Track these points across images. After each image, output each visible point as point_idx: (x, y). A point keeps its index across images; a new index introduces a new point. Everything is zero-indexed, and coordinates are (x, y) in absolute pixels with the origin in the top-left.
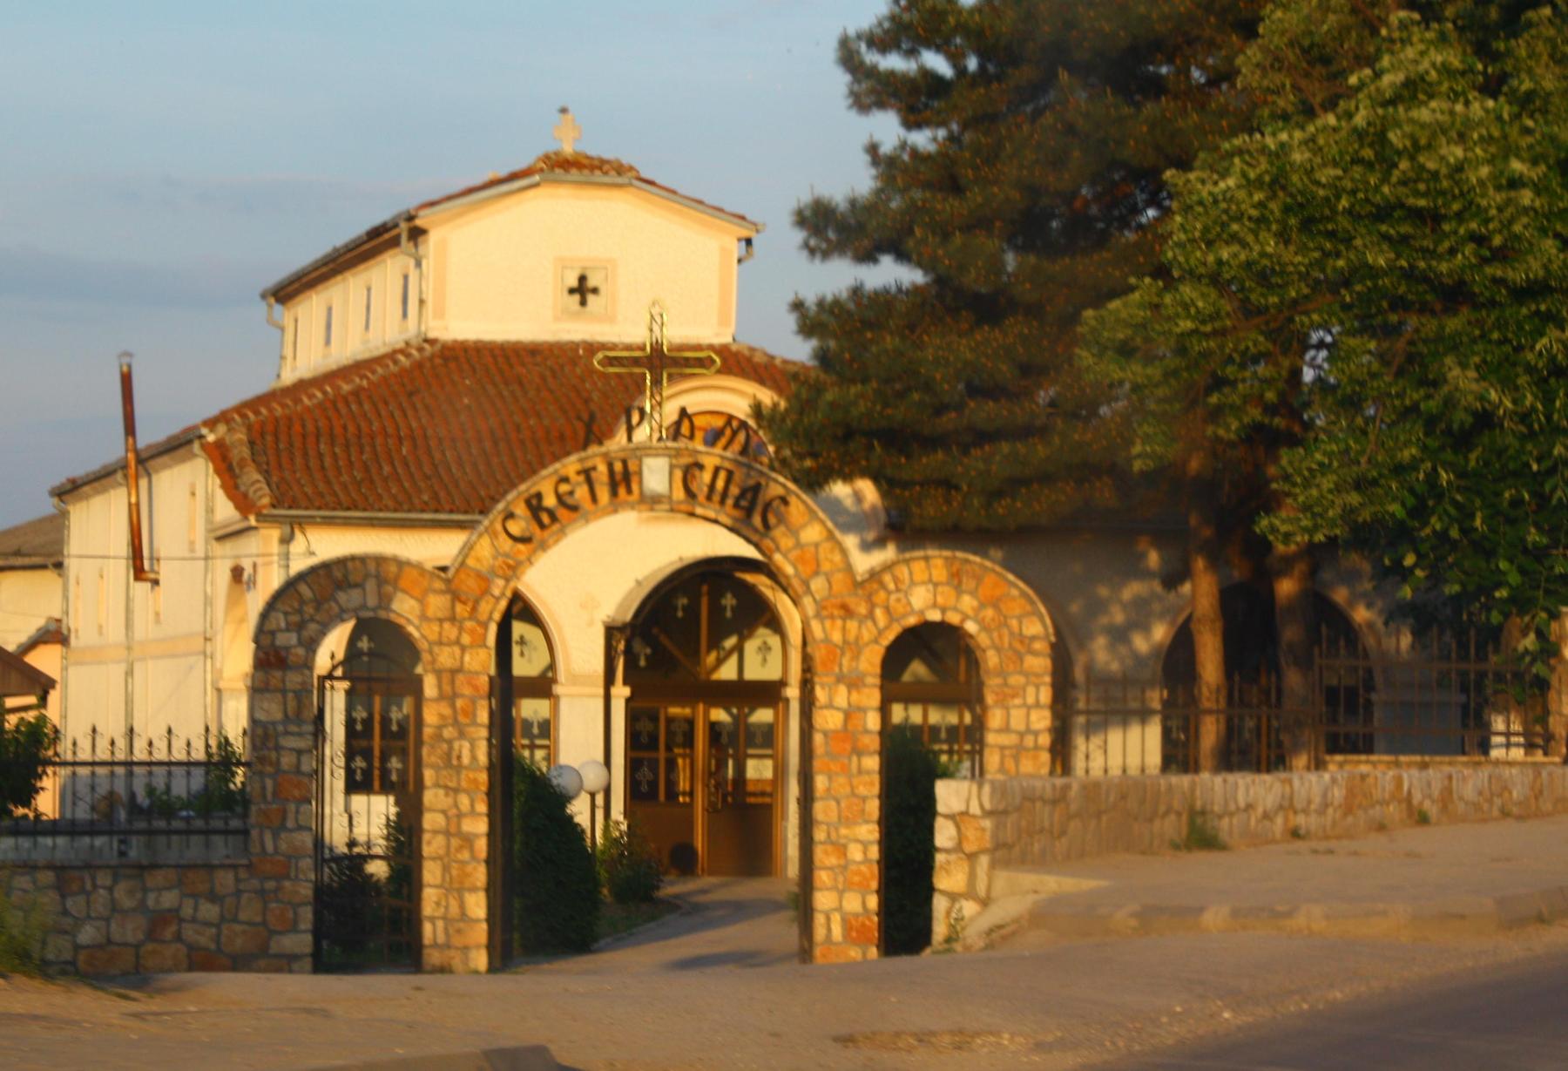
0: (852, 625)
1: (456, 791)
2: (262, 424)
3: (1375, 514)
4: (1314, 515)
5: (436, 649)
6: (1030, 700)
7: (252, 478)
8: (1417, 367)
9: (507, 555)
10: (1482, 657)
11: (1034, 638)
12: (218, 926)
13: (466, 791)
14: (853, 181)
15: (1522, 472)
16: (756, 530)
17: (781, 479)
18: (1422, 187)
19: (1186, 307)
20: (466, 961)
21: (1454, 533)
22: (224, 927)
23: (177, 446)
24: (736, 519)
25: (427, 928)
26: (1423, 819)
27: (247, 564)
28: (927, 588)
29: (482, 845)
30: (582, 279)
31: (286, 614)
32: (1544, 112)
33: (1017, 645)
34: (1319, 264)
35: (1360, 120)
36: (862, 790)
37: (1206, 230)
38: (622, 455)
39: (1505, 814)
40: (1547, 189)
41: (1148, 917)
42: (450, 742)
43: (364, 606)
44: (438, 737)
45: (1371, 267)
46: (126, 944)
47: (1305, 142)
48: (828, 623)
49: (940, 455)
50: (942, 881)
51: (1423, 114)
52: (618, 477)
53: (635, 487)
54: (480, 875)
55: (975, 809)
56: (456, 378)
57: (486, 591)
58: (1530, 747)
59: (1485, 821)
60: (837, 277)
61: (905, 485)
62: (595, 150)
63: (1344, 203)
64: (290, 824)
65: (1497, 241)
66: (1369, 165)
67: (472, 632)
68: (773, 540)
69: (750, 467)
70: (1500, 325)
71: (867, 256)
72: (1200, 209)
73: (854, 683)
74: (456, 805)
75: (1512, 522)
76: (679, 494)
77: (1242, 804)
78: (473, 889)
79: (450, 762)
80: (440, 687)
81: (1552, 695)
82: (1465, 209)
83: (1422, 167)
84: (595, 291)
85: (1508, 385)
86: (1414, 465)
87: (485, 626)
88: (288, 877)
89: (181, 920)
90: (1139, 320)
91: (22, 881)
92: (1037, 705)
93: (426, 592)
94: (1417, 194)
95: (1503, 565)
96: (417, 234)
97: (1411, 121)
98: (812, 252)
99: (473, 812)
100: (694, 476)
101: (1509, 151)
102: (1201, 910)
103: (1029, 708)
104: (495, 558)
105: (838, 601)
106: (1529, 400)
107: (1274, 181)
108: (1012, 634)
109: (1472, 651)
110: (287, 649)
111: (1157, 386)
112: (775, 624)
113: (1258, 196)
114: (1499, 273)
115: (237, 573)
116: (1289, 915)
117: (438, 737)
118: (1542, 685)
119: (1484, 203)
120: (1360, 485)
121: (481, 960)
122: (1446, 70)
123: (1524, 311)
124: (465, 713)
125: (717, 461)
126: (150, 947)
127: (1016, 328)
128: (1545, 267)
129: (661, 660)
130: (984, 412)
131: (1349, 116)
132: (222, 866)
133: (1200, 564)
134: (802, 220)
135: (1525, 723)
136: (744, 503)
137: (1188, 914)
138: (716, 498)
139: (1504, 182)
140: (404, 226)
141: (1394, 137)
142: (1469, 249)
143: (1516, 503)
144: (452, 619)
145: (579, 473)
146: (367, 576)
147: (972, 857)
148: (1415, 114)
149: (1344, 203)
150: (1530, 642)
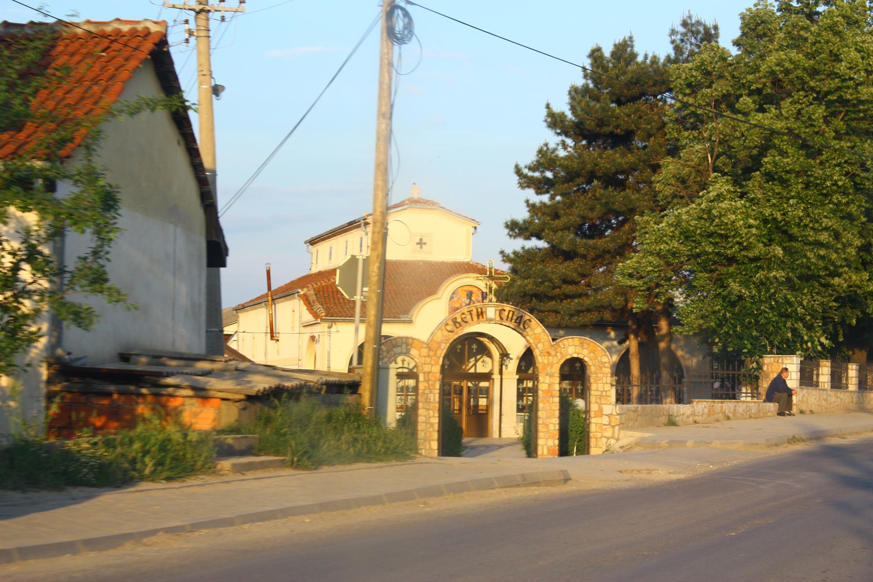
0: (550, 358)
1: (429, 409)
2: (319, 288)
7: (318, 306)
10: (739, 370)
14: (522, 215)
15: (751, 314)
19: (650, 263)
21: (731, 332)
23: (287, 292)
26: (728, 418)
27: (316, 335)
28: (573, 346)
29: (436, 427)
30: (421, 239)
32: (758, 204)
34: (691, 250)
36: (554, 408)
41: (671, 443)
44: (424, 393)
49: (554, 302)
51: (723, 205)
55: (614, 413)
57: (439, 347)
58: (753, 397)
60: (519, 244)
61: (542, 312)
62: (424, 196)
63: (698, 231)
65: (745, 244)
66: (706, 220)
70: (745, 270)
71: (528, 238)
73: (551, 376)
75: (748, 328)
76: (498, 318)
79: (427, 401)
81: (760, 381)
84: (425, 244)
85: (747, 287)
86: (719, 311)
87: (439, 358)
94: (721, 229)
95: (746, 342)
97: (720, 207)
98: (511, 236)
99: (434, 416)
101: (748, 216)
112: (490, 355)
113: (672, 229)
115: (313, 338)
117: (424, 393)
118: (757, 378)
122: (729, 191)
127: (578, 261)
130: (569, 289)
131: (700, 205)
133: (632, 337)
134: (507, 226)
137: (682, 443)
141: (714, 211)
143: (750, 323)
144: (429, 356)
148: (720, 205)
149: (698, 231)
150: (754, 365)
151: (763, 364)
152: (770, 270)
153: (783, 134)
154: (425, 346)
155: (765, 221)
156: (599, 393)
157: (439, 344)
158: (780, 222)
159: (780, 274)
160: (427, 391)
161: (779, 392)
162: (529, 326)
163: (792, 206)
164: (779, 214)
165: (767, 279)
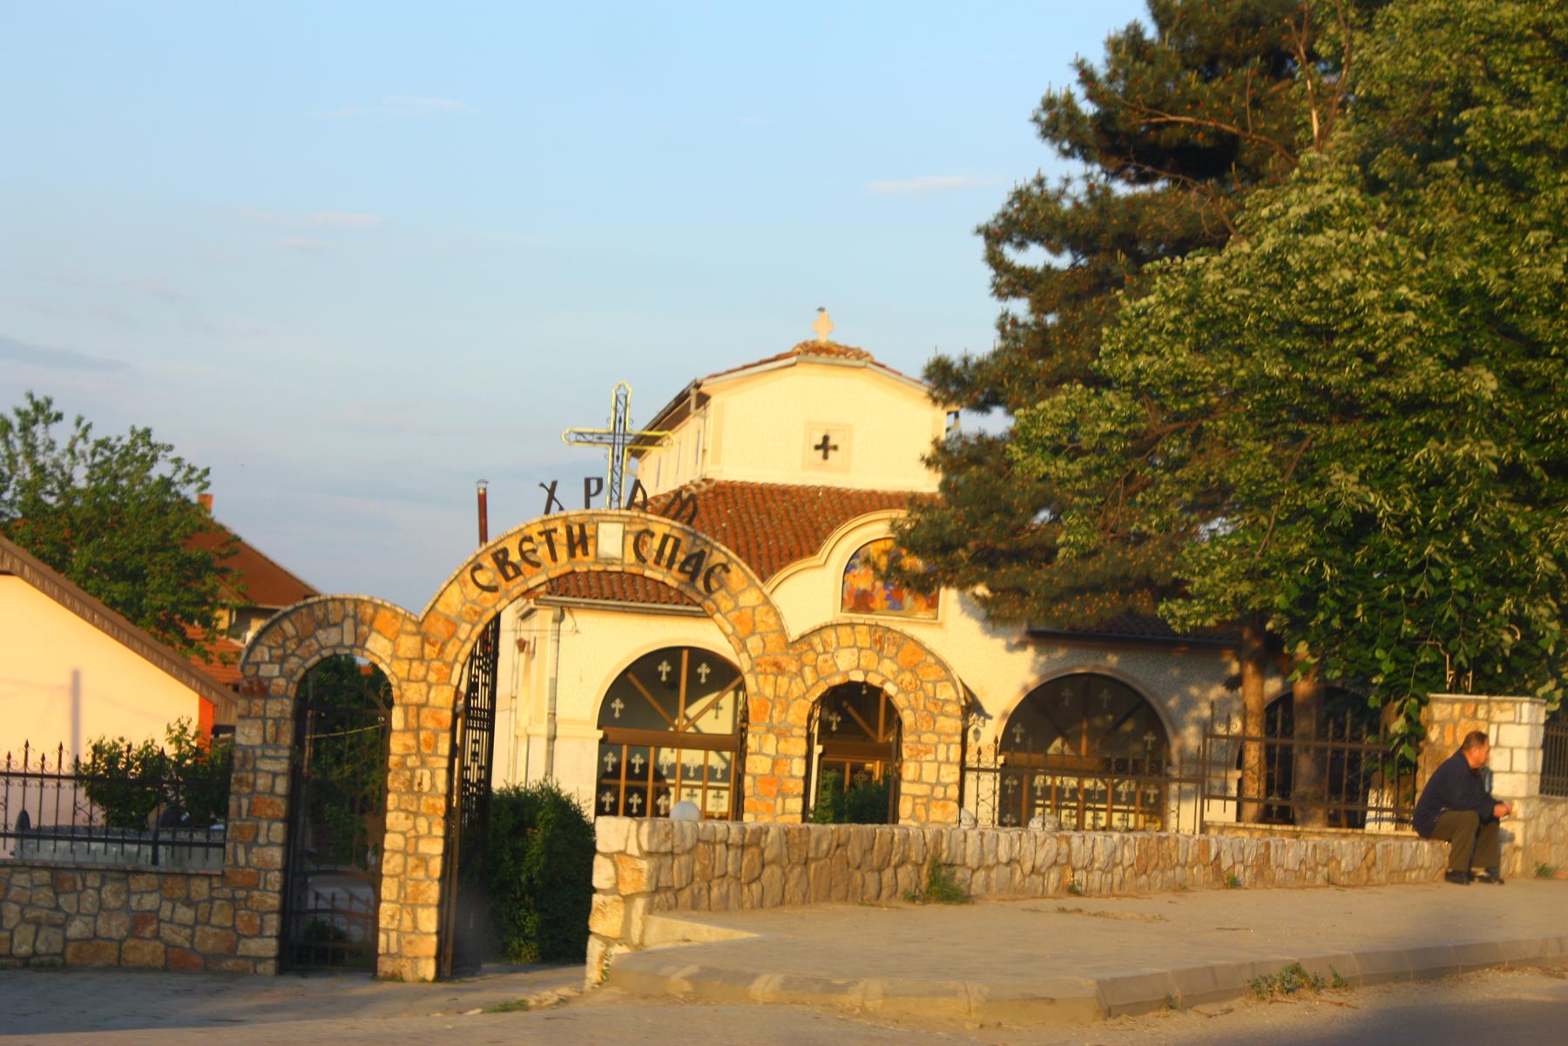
0: (783, 681)
1: (416, 814)
3: (1263, 602)
4: (1207, 602)
5: (404, 685)
6: (942, 757)
8: (1308, 473)
9: (474, 602)
11: (946, 701)
12: (192, 928)
13: (424, 815)
16: (699, 593)
17: (724, 548)
18: (1315, 305)
19: (1110, 410)
20: (415, 970)
22: (198, 928)
24: (681, 583)
25: (382, 938)
26: (1234, 884)
29: (436, 866)
30: (826, 438)
31: (270, 648)
33: (931, 707)
35: (1268, 246)
37: (1128, 342)
38: (580, 520)
39: (1330, 882)
40: (1433, 315)
42: (413, 770)
43: (341, 644)
44: (403, 765)
45: (1270, 378)
46: (111, 939)
47: (1221, 267)
48: (761, 678)
50: (597, 924)
51: (1319, 240)
52: (576, 540)
53: (591, 549)
54: (433, 892)
55: (633, 849)
56: (721, 508)
59: (1303, 888)
63: (1251, 319)
64: (261, 840)
65: (1382, 357)
67: (438, 671)
68: (714, 602)
69: (695, 536)
71: (982, 407)
72: (1125, 323)
73: (782, 734)
74: (415, 827)
77: (1004, 859)
78: (426, 906)
79: (413, 788)
80: (406, 721)
82: (1353, 329)
83: (1315, 286)
85: (1390, 491)
86: (1300, 560)
88: (256, 888)
89: (160, 921)
90: (1066, 421)
91: (21, 879)
92: (948, 761)
93: (398, 634)
95: (1379, 654)
96: (703, 400)
98: (935, 401)
100: (645, 543)
102: (755, 976)
103: (940, 764)
104: (463, 604)
105: (770, 659)
106: (1408, 504)
107: (1191, 300)
108: (927, 697)
109: (1279, 725)
110: (270, 679)
111: (1077, 480)
113: (1175, 312)
114: (1383, 386)
116: (843, 989)
117: (403, 765)
119: (1372, 322)
120: (1252, 574)
121: (429, 969)
123: (1407, 424)
124: (428, 745)
125: (667, 530)
126: (131, 942)
128: (1424, 381)
129: (847, 725)
132: (197, 875)
135: (1396, 801)
136: (688, 568)
138: (664, 563)
139: (1392, 305)
140: (693, 392)
142: (1356, 362)
143: (1394, 597)
144: (422, 658)
145: (541, 534)
146: (345, 617)
147: (628, 899)
149: (1251, 319)
151: (1430, 721)
152: (1457, 435)
153: (1521, 39)
154: (410, 627)
155: (1454, 297)
156: (925, 790)
157: (453, 625)
158: (1497, 299)
159: (1486, 452)
160: (411, 761)
161: (1454, 808)
162: (721, 586)
163: (1532, 251)
164: (1493, 274)
165: (1448, 464)
